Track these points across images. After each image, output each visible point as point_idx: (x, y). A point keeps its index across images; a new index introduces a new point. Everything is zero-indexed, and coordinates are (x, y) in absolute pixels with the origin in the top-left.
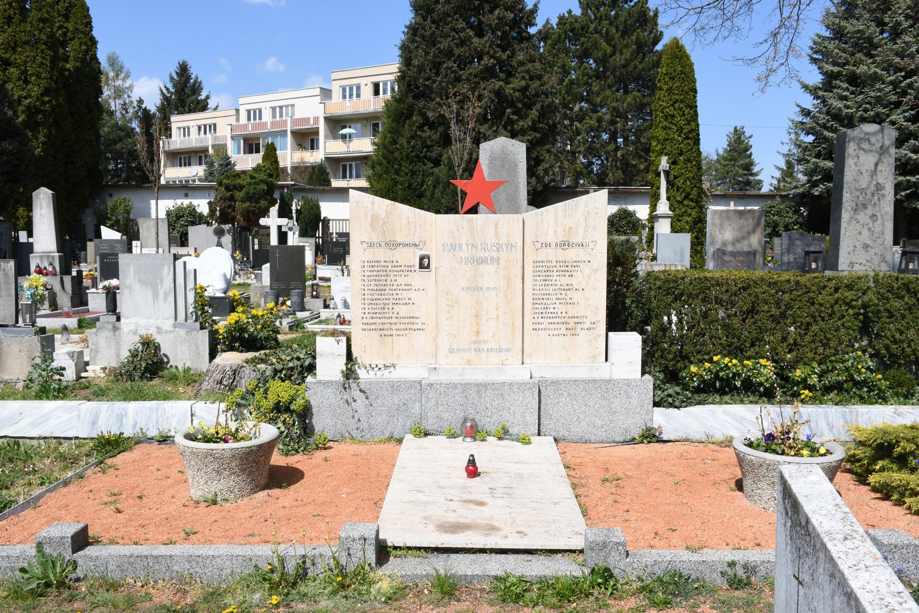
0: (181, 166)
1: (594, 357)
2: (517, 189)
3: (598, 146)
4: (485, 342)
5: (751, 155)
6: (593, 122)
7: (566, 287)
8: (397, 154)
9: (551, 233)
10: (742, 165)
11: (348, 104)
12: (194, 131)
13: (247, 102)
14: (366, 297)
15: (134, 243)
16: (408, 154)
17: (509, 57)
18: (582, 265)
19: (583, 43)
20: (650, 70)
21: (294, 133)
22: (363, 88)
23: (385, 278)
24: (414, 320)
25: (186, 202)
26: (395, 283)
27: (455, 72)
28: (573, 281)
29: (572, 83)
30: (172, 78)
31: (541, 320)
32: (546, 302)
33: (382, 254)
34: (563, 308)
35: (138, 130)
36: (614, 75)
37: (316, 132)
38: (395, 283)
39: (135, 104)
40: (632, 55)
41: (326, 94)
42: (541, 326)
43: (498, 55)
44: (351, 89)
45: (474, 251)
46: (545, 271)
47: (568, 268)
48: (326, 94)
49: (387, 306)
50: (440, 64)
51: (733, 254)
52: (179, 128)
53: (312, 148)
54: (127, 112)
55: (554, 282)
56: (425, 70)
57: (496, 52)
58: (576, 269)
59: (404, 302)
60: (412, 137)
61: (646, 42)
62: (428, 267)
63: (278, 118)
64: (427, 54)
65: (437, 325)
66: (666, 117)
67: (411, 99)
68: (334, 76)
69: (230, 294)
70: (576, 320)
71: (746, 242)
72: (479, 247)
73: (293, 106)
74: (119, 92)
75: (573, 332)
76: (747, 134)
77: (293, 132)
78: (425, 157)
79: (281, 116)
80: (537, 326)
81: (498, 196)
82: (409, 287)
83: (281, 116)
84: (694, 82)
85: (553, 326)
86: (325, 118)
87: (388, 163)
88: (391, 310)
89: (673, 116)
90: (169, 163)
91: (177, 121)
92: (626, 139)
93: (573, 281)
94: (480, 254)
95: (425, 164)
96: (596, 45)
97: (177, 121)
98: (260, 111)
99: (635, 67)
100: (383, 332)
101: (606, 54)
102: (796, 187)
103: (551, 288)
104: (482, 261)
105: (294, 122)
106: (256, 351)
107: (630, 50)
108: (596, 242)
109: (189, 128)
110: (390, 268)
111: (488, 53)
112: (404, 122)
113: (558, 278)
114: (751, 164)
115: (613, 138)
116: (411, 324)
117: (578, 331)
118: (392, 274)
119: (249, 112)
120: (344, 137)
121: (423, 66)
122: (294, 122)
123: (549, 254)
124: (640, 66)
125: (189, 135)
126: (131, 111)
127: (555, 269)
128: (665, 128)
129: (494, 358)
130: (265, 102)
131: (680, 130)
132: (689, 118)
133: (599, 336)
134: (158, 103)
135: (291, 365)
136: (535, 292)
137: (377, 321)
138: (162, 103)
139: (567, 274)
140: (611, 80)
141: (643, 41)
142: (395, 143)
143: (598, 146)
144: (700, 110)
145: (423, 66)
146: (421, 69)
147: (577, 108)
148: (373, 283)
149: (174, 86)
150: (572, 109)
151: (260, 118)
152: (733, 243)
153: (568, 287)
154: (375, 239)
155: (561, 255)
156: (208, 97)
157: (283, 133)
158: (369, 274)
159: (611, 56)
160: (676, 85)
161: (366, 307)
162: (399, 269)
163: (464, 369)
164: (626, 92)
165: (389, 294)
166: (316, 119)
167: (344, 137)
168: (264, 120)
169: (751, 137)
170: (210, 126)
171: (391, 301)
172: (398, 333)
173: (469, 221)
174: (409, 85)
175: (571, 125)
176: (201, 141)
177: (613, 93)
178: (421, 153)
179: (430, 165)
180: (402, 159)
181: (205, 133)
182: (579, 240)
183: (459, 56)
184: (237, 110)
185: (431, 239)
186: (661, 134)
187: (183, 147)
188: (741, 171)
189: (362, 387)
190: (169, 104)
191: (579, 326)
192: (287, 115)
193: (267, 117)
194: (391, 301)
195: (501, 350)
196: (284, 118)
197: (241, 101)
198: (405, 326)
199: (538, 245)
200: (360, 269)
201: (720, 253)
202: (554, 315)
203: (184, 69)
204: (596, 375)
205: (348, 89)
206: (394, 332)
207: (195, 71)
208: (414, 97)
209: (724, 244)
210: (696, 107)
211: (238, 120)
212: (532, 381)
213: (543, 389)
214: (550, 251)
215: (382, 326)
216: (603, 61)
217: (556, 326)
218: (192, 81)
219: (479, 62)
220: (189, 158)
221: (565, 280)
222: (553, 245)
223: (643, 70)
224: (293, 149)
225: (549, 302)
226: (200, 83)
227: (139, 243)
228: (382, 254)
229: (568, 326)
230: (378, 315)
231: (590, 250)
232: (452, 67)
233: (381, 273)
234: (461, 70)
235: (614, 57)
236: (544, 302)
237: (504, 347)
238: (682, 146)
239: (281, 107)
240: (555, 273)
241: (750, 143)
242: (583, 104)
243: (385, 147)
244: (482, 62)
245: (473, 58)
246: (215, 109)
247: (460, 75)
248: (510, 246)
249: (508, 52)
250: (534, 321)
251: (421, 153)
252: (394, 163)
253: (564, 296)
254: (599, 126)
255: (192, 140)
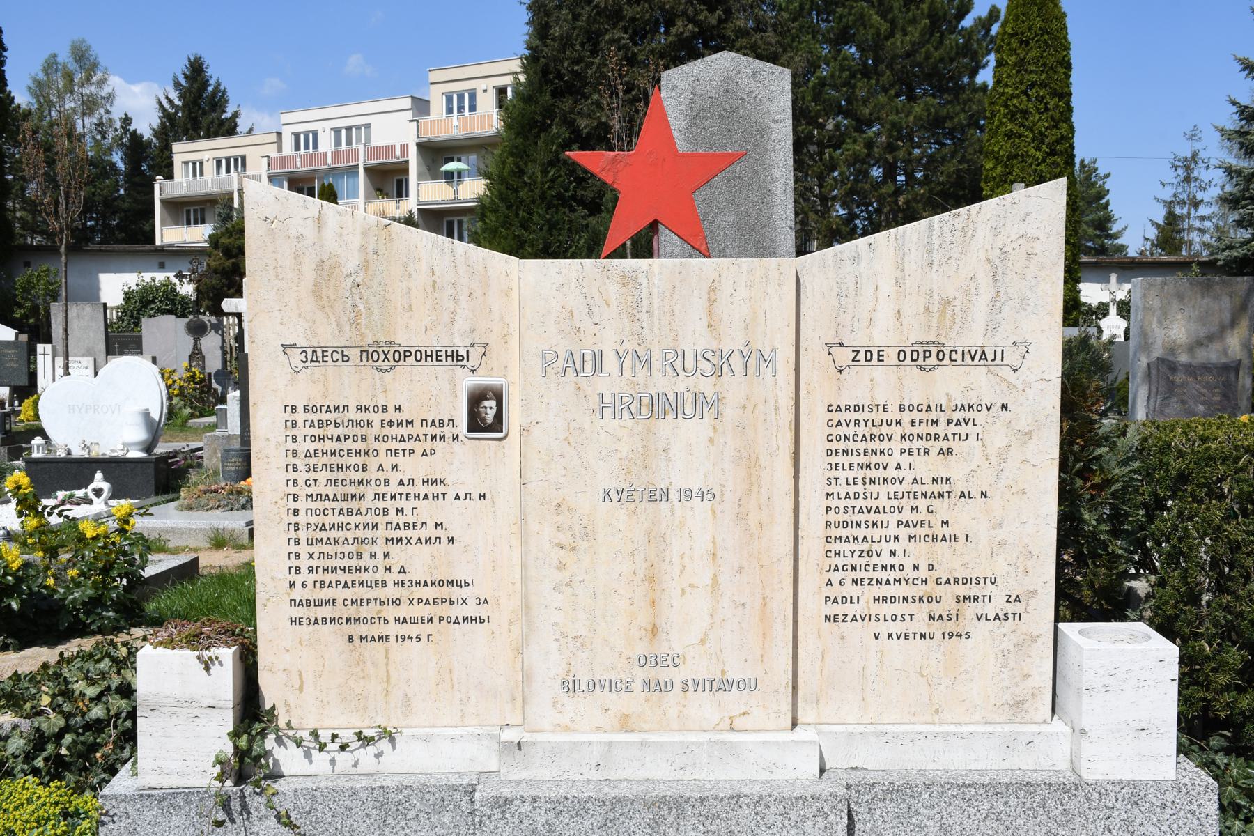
0: (189, 223)
1: (1018, 705)
2: (766, 196)
3: (867, 187)
4: (676, 661)
5: (1107, 204)
6: (859, 148)
7: (930, 488)
8: (523, 193)
9: (885, 316)
10: (1093, 221)
11: (455, 122)
12: (210, 168)
13: (295, 121)
14: (302, 519)
15: (40, 347)
16: (544, 193)
17: (720, 21)
18: (980, 417)
19: (841, 17)
20: (952, 60)
21: (369, 170)
22: (480, 97)
23: (359, 460)
24: (455, 592)
25: (160, 277)
26: (394, 477)
27: (626, 47)
28: (956, 469)
29: (822, 83)
30: (177, 85)
31: (850, 590)
32: (869, 532)
33: (351, 386)
34: (919, 553)
35: (121, 166)
36: (892, 70)
37: (403, 169)
38: (394, 477)
39: (118, 124)
40: (922, 35)
41: (421, 107)
42: (850, 609)
43: (701, 17)
44: (461, 98)
45: (642, 374)
46: (862, 437)
47: (938, 428)
48: (421, 107)
49: (367, 549)
50: (599, 34)
51: (1191, 370)
52: (186, 163)
53: (400, 195)
54: (104, 138)
55: (891, 473)
56: (572, 46)
57: (697, 12)
58: (962, 430)
59: (423, 534)
60: (551, 163)
61: (945, 14)
62: (498, 424)
63: (344, 146)
64: (576, 17)
65: (527, 607)
66: (1012, 116)
67: (548, 97)
68: (433, 77)
69: (160, 450)
70: (961, 590)
71: (1216, 346)
72: (657, 363)
73: (368, 126)
74: (90, 105)
75: (951, 626)
76: (1101, 172)
77: (366, 169)
78: (574, 197)
79: (349, 142)
80: (839, 609)
81: (713, 201)
82: (439, 489)
83: (349, 142)
84: (1067, 48)
85: (887, 609)
86: (418, 145)
87: (508, 208)
88: (380, 562)
89: (1025, 113)
90: (169, 220)
91: (183, 152)
92: (910, 176)
93: (956, 469)
94: (661, 384)
95: (573, 211)
96: (862, 19)
97: (183, 152)
98: (315, 134)
99: (928, 57)
100: (359, 629)
101: (878, 34)
102: (1230, 247)
103: (883, 489)
104: (664, 407)
105: (370, 152)
106: (52, 644)
107: (919, 27)
108: (1027, 345)
109: (201, 163)
110: (376, 429)
111: (684, 13)
112: (537, 136)
113: (905, 460)
114: (1108, 219)
115: (890, 173)
116: (447, 605)
117: (968, 621)
118: (382, 447)
119: (297, 136)
120: (449, 176)
121: (569, 37)
122: (370, 152)
123: (882, 385)
124: (937, 54)
125: (202, 174)
126: (111, 135)
127: (896, 431)
128: (1009, 135)
129: (704, 708)
130: (323, 120)
131: (1040, 138)
132: (1057, 116)
133: (1035, 639)
134: (156, 123)
135: (97, 712)
136: (833, 503)
137: (339, 594)
138: (163, 125)
139: (935, 446)
140: (887, 77)
141: (941, 13)
142: (522, 172)
143: (867, 187)
144: (1075, 101)
145: (569, 37)
146: (566, 43)
147: (830, 126)
148: (323, 476)
149: (181, 97)
150: (821, 127)
151: (316, 146)
152: (1191, 349)
153: (936, 488)
154: (327, 337)
155: (917, 386)
156: (236, 115)
157: (353, 171)
158: (312, 447)
159: (887, 38)
160: (1033, 54)
161: (304, 549)
162: (404, 431)
163: (610, 745)
164: (912, 98)
165: (375, 511)
166: (405, 147)
167: (449, 176)
168: (321, 149)
169: (1107, 176)
170: (236, 160)
171: (381, 533)
172: (405, 629)
173: (624, 279)
174: (545, 72)
175: (821, 154)
176: (221, 183)
177: (891, 99)
178: (567, 190)
179: (583, 212)
180: (533, 202)
181: (228, 171)
182: (974, 338)
183: (633, 19)
184: (279, 134)
185: (505, 337)
186: (1003, 147)
187: (191, 193)
188: (1091, 231)
189: (285, 805)
190: (173, 125)
191: (971, 609)
192: (359, 141)
193: (326, 144)
194: (381, 533)
195: (726, 685)
196: (354, 146)
197: (286, 118)
198: (425, 611)
199: (844, 356)
200: (280, 432)
201: (1163, 369)
202: (892, 575)
203: (196, 70)
204: (1024, 763)
205: (455, 97)
206: (392, 629)
207: (215, 73)
208: (554, 94)
209: (1172, 350)
210: (1070, 94)
211: (280, 149)
212: (824, 788)
213: (860, 811)
214: (878, 372)
215: (352, 611)
216: (874, 47)
217: (899, 609)
218: (210, 89)
219: (667, 32)
220: (203, 210)
221: (927, 467)
222: (891, 356)
223: (942, 60)
224: (367, 197)
225: (877, 533)
226: (225, 91)
227: (48, 347)
228: (351, 386)
229: (937, 609)
230: (342, 576)
231: (1006, 372)
232: (621, 38)
233: (349, 444)
234: (636, 44)
235: (892, 40)
236: (861, 533)
237: (734, 674)
238: (1042, 167)
239: (349, 129)
240: (896, 445)
241: (1107, 187)
242: (839, 118)
243: (503, 180)
244: (673, 30)
245: (657, 24)
246: (251, 130)
247: (635, 54)
248: (756, 360)
249: (719, 12)
250: (827, 591)
251: (567, 190)
252: (518, 208)
253: (922, 515)
254: (868, 155)
255: (206, 182)
